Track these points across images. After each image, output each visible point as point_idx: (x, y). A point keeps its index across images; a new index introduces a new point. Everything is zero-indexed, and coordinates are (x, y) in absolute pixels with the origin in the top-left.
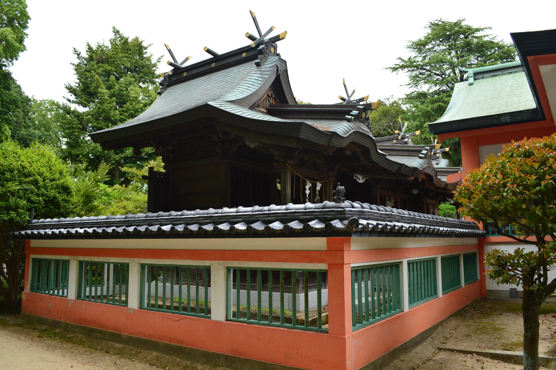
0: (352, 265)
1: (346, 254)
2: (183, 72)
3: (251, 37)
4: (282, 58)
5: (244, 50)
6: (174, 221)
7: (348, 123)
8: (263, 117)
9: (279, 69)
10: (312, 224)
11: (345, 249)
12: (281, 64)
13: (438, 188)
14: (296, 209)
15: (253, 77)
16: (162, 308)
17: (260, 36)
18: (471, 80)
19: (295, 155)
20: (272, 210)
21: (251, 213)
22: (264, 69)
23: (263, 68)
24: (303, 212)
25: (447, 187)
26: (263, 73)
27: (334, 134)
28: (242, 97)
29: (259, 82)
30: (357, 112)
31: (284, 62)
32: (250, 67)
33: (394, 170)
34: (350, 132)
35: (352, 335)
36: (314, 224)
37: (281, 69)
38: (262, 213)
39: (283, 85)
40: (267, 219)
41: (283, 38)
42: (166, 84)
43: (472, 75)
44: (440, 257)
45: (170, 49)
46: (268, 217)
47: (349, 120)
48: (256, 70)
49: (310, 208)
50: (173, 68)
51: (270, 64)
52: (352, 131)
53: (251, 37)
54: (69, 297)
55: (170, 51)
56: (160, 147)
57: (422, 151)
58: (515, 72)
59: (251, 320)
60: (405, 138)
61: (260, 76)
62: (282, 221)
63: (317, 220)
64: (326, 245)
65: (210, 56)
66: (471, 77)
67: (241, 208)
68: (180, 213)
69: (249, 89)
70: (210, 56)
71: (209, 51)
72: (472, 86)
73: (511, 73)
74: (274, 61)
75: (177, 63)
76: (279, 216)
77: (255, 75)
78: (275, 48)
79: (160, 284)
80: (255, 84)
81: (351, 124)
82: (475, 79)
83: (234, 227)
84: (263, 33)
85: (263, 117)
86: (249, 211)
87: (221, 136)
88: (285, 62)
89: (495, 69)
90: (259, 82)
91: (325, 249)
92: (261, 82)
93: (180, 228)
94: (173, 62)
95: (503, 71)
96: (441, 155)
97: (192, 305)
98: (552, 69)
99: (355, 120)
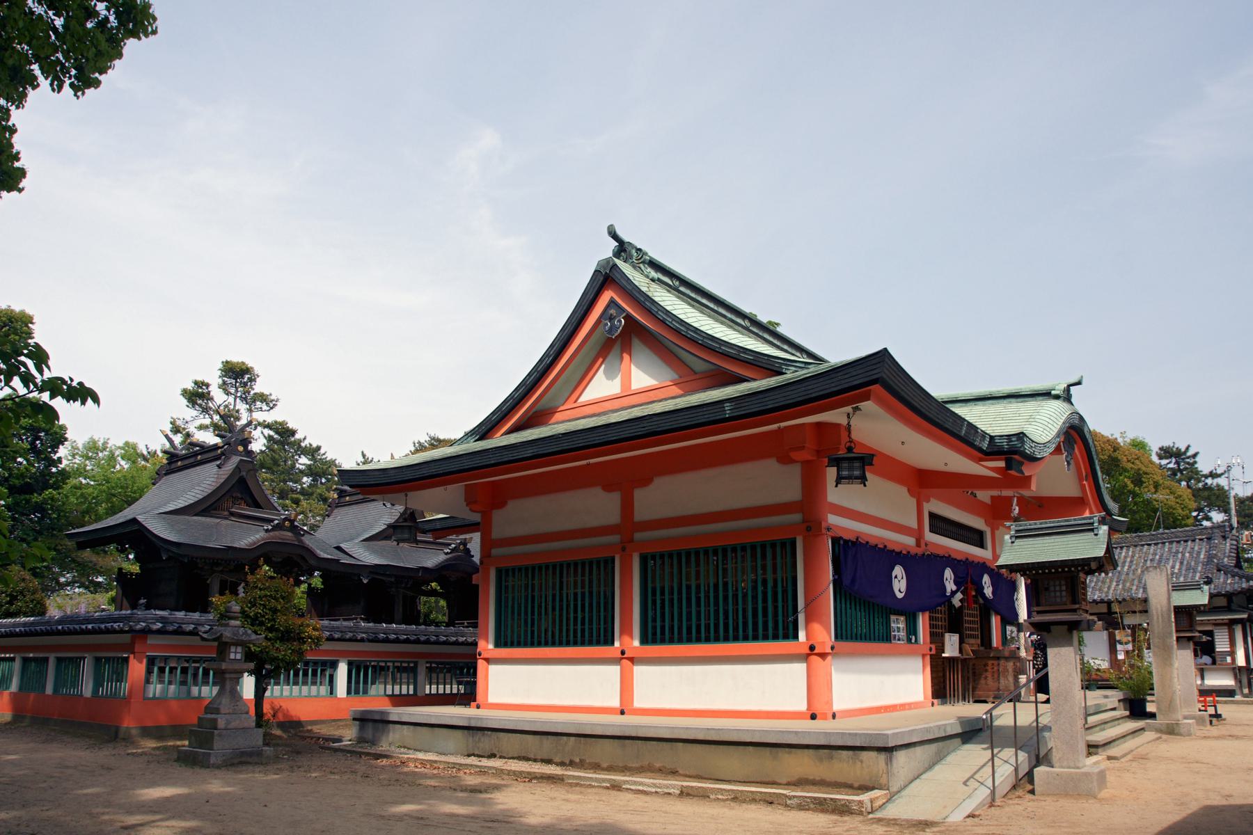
0: (148, 654)
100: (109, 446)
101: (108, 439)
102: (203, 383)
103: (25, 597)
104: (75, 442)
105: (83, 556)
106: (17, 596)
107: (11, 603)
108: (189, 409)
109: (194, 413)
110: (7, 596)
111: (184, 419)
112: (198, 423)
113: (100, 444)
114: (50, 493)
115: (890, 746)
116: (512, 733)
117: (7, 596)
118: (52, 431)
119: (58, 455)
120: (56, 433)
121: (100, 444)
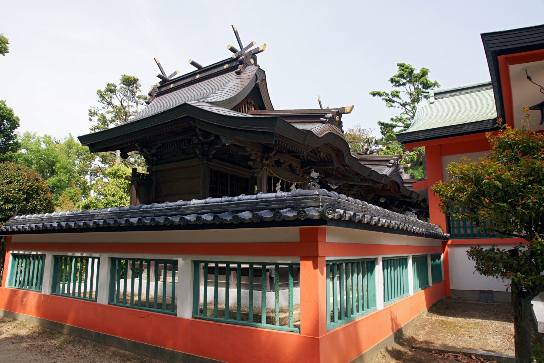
0: (327, 258)
1: (320, 245)
2: (170, 84)
3: (233, 50)
4: (261, 68)
5: (226, 61)
6: (143, 214)
7: (323, 125)
8: (239, 114)
9: (258, 76)
10: (283, 212)
11: (319, 240)
12: (260, 73)
13: (404, 196)
14: (267, 198)
15: (233, 84)
16: (162, 309)
17: (241, 49)
18: (432, 99)
19: (271, 155)
20: (242, 200)
21: (220, 203)
22: (243, 77)
23: (242, 76)
24: (275, 200)
25: (411, 196)
26: (242, 80)
27: (310, 132)
28: (221, 100)
29: (239, 88)
30: (331, 115)
31: (263, 73)
32: (232, 75)
33: (366, 174)
34: (325, 133)
35: (327, 336)
36: (286, 212)
37: (260, 78)
38: (231, 203)
39: (262, 94)
40: (236, 209)
41: (262, 51)
42: (155, 94)
43: (433, 95)
44: (411, 256)
45: (159, 63)
46: (237, 207)
47: (323, 123)
48: (236, 78)
49: (282, 196)
50: (161, 80)
51: (249, 72)
52: (327, 132)
53: (233, 50)
54: (99, 302)
55: (159, 65)
56: (144, 150)
57: (390, 161)
58: (472, 92)
59: (219, 319)
60: (373, 153)
61: (240, 83)
62: (251, 211)
63: (289, 209)
64: (298, 236)
65: (195, 69)
66: (433, 96)
67: (210, 200)
68: (150, 206)
69: (229, 93)
70: (195, 69)
71: (193, 64)
72: (433, 104)
73: (468, 93)
74: (253, 70)
75: (166, 76)
76: (249, 206)
77: (234, 82)
78: (255, 60)
79: (129, 281)
80: (234, 90)
81: (326, 126)
82: (436, 99)
83: (201, 218)
84: (244, 46)
85: (239, 114)
86: (218, 201)
87: (200, 138)
88: (264, 72)
89: (453, 90)
90: (239, 88)
91: (298, 240)
92: (240, 88)
93: (147, 220)
94: (161, 74)
95: (460, 92)
96: (403, 170)
97: (160, 301)
98: (522, 70)
99: (329, 122)
100: (36, 136)
101: (36, 133)
102: (112, 85)
103: (39, 195)
104: (19, 132)
105: (92, 162)
106: (33, 194)
107: (27, 200)
108: (100, 103)
109: (103, 105)
110: (24, 193)
111: (97, 108)
112: (106, 110)
113: (32, 134)
114: (10, 154)
115: (128, 280)
116: (126, 286)
117: (24, 193)
118: (12, 119)
119: (14, 133)
120: (14, 120)
121: (32, 134)
